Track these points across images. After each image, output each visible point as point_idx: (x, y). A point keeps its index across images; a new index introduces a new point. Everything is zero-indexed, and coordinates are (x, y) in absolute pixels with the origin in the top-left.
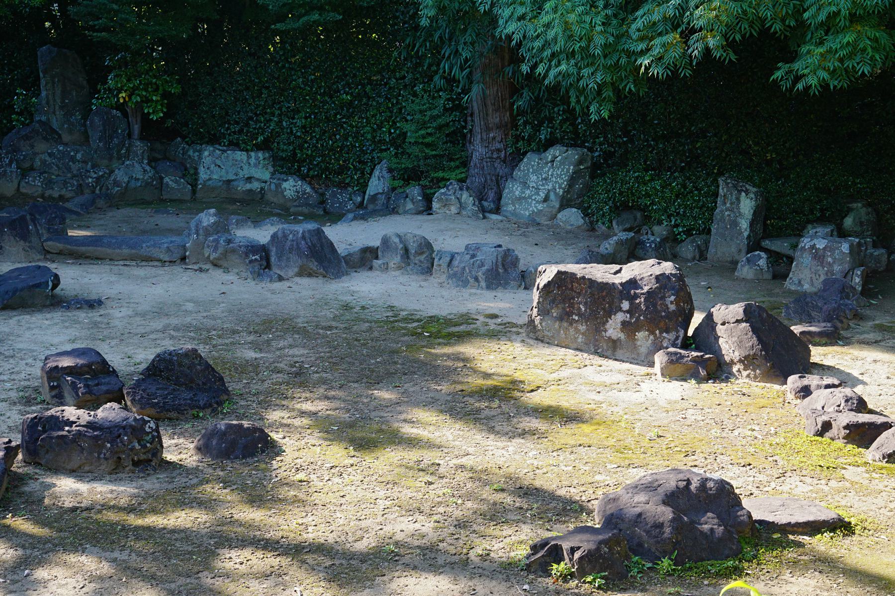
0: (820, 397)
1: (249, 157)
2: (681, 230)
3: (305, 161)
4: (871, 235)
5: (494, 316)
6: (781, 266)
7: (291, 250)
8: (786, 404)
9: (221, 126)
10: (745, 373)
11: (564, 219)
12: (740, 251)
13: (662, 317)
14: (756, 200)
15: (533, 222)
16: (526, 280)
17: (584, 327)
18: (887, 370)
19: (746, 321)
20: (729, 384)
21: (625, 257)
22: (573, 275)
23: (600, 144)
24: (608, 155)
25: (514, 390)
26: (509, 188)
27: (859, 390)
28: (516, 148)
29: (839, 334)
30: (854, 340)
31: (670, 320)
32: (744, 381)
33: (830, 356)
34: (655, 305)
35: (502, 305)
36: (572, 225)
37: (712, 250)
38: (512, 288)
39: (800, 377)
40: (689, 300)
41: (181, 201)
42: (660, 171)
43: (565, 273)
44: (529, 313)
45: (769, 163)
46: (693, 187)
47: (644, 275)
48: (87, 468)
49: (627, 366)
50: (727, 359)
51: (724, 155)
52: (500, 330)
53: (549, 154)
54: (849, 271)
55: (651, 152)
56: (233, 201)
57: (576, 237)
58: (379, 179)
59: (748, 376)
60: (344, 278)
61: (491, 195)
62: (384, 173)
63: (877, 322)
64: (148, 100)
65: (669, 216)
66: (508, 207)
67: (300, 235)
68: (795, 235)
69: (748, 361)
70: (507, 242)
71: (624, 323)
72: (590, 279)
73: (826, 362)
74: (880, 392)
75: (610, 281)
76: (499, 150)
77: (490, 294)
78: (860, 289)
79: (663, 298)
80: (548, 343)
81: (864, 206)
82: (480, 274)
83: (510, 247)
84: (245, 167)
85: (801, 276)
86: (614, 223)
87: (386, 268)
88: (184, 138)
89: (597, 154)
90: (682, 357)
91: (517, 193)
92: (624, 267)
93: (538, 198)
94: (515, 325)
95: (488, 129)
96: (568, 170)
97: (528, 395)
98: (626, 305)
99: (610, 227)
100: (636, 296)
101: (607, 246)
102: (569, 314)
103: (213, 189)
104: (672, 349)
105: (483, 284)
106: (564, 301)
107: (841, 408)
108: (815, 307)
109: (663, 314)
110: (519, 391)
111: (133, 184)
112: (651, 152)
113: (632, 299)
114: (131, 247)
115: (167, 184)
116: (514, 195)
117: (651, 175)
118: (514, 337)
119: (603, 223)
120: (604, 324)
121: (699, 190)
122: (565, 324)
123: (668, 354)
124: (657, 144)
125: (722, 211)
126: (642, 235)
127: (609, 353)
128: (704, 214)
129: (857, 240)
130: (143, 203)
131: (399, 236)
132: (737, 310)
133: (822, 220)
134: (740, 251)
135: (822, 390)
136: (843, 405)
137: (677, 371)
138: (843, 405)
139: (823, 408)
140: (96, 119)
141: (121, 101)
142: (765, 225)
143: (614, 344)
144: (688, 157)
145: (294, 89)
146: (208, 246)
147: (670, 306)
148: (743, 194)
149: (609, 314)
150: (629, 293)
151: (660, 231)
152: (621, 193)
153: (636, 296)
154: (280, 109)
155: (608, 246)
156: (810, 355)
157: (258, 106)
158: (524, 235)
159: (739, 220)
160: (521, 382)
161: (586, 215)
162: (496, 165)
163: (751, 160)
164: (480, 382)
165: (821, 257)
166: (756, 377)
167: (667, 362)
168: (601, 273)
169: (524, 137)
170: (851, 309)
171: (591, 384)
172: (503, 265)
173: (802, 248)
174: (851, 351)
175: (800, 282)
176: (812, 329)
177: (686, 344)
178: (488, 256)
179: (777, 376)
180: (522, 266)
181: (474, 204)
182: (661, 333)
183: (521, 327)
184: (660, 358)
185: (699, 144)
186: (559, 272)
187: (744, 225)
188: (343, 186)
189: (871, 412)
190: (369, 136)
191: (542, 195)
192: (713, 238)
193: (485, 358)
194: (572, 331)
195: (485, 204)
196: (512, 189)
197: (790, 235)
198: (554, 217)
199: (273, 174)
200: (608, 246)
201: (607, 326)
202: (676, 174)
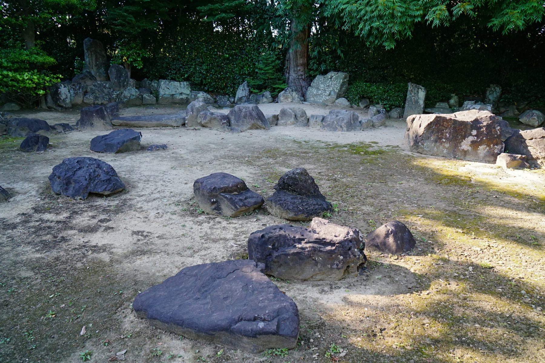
1: (180, 84)
3: (207, 84)
7: (245, 117)
9: (167, 71)
34: (491, 131)
41: (153, 105)
43: (440, 117)
47: (482, 116)
48: (319, 277)
53: (329, 75)
56: (176, 103)
58: (243, 90)
62: (246, 87)
64: (135, 60)
67: (251, 109)
76: (302, 75)
82: (343, 124)
84: (179, 89)
87: (286, 125)
88: (148, 78)
95: (297, 66)
96: (340, 82)
100: (481, 127)
102: (440, 139)
103: (166, 98)
105: (345, 129)
111: (132, 97)
114: (158, 120)
115: (145, 98)
120: (460, 143)
130: (136, 105)
131: (291, 109)
140: (113, 70)
141: (124, 61)
145: (202, 53)
146: (200, 117)
149: (464, 137)
153: (481, 127)
154: (195, 62)
157: (185, 61)
159: (419, 100)
182: (493, 146)
186: (437, 117)
187: (422, 102)
188: (225, 94)
190: (238, 72)
191: (328, 93)
194: (441, 147)
198: (334, 102)
199: (191, 91)
201: (462, 144)
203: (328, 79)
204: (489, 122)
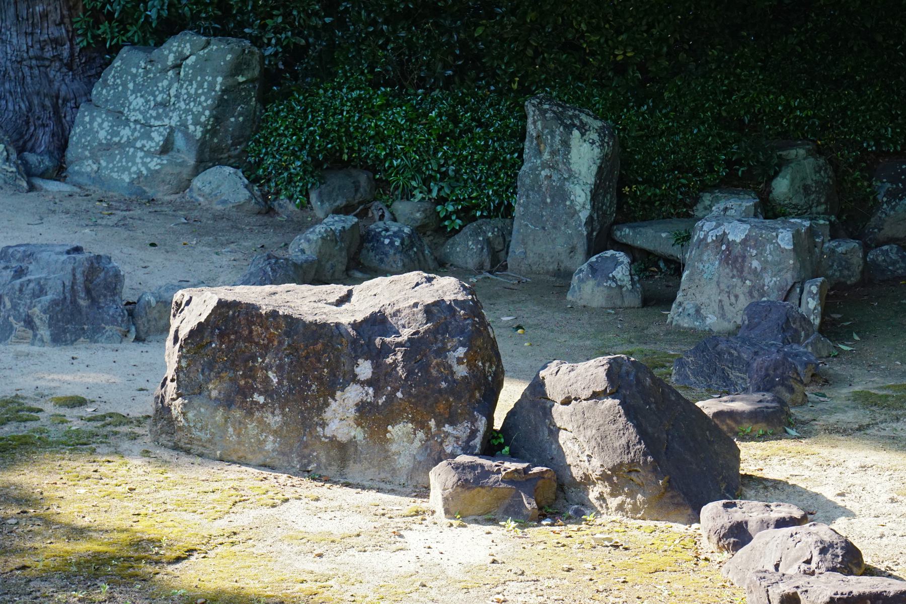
0: (768, 545)
2: (451, 208)
4: (825, 212)
5: (78, 402)
6: (658, 279)
8: (702, 563)
10: (614, 502)
11: (207, 190)
12: (573, 250)
13: (440, 391)
14: (601, 146)
15: (140, 197)
16: (142, 321)
17: (278, 418)
18: (888, 485)
19: (613, 395)
20: (583, 526)
21: (341, 267)
22: (251, 309)
23: (277, 30)
24: (293, 54)
25: (139, 560)
26: (83, 124)
27: (841, 524)
28: (94, 37)
29: (789, 415)
30: (818, 425)
31: (458, 398)
32: (613, 519)
33: (775, 460)
34: (425, 368)
35: (92, 378)
36: (224, 202)
37: (516, 249)
38: (109, 339)
39: (726, 506)
40: (495, 356)
42: (402, 87)
43: (235, 304)
44: (159, 391)
45: (620, 69)
46: (473, 119)
47: (401, 305)
49: (371, 496)
50: (577, 473)
51: (530, 52)
52: (96, 434)
54: (793, 286)
55: (383, 47)
57: (235, 227)
59: (620, 508)
60: (82, 342)
61: (44, 139)
63: (857, 388)
65: (426, 181)
66: (84, 165)
68: (678, 215)
69: (618, 477)
70: (94, 241)
71: (361, 407)
72: (286, 317)
73: (771, 473)
74: (881, 530)
75: (331, 320)
76: (56, 42)
77: (59, 354)
78: (817, 322)
79: (442, 352)
80: (201, 455)
81: (809, 153)
82: (37, 310)
83: (97, 250)
85: (701, 299)
86: (313, 197)
89: (270, 51)
90: (487, 473)
91: (102, 134)
92: (356, 289)
93: (149, 145)
94: (124, 420)
97: (170, 568)
98: (365, 369)
99: (305, 206)
100: (386, 350)
101: (305, 246)
102: (245, 392)
104: (464, 459)
105: (45, 332)
106: (232, 365)
107: (813, 566)
108: (735, 361)
109: (444, 385)
110: (150, 561)
112: (383, 47)
113: (377, 355)
116: (95, 138)
117: (385, 94)
118: (126, 445)
119: (290, 198)
121: (485, 126)
122: (238, 414)
123: (456, 467)
124: (395, 31)
125: (534, 169)
126: (373, 220)
127: (332, 471)
128: (497, 175)
129: (807, 224)
132: (592, 372)
133: (731, 184)
134: (573, 250)
135: (772, 531)
136: (816, 559)
137: (478, 504)
138: (816, 559)
139: (777, 567)
142: (620, 195)
143: (343, 451)
144: (457, 58)
147: (456, 368)
148: (576, 133)
149: (331, 388)
150: (371, 342)
151: (410, 210)
152: (325, 134)
153: (386, 350)
155: (305, 245)
156: (738, 460)
158: (123, 224)
159: (569, 186)
160: (151, 541)
161: (254, 180)
162: (52, 74)
163: (586, 63)
164: (61, 546)
165: (739, 260)
166: (635, 510)
167: (456, 485)
168: (309, 302)
169: (110, 15)
170: (806, 364)
171: (302, 539)
172: (88, 292)
173: (700, 241)
174: (815, 448)
175: (698, 311)
176: (739, 405)
177: (492, 447)
178: (53, 273)
179: (678, 505)
180: (128, 295)
181: (7, 159)
182: (439, 425)
183: (139, 422)
184: (440, 478)
185: (479, 31)
186: (221, 304)
187: (580, 196)
189: (870, 571)
191: (158, 138)
192: (520, 225)
193: (68, 493)
194: (252, 427)
195: (32, 158)
196: (91, 127)
197: (669, 216)
198: (184, 186)
200: (305, 245)
201: (328, 414)
202: (436, 93)
203: (165, 71)
204: (422, 329)
